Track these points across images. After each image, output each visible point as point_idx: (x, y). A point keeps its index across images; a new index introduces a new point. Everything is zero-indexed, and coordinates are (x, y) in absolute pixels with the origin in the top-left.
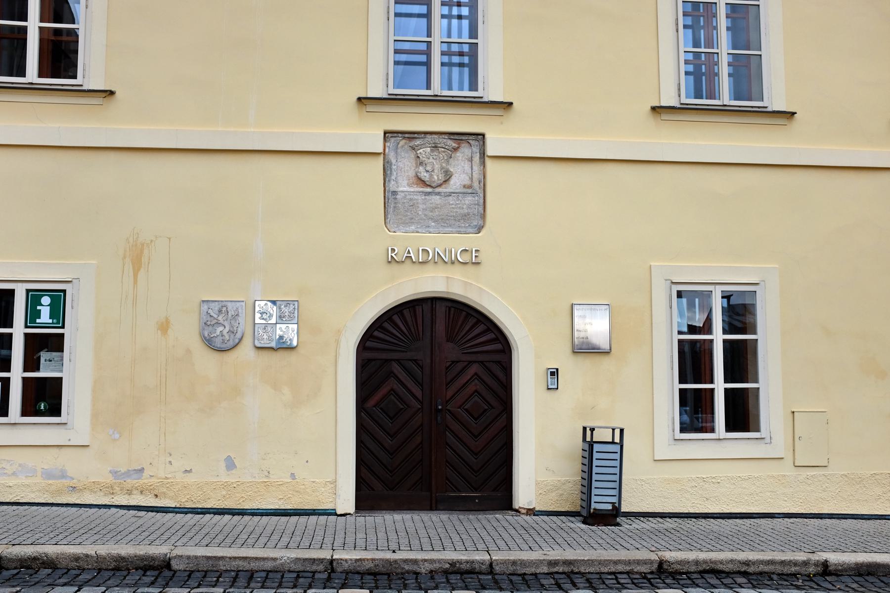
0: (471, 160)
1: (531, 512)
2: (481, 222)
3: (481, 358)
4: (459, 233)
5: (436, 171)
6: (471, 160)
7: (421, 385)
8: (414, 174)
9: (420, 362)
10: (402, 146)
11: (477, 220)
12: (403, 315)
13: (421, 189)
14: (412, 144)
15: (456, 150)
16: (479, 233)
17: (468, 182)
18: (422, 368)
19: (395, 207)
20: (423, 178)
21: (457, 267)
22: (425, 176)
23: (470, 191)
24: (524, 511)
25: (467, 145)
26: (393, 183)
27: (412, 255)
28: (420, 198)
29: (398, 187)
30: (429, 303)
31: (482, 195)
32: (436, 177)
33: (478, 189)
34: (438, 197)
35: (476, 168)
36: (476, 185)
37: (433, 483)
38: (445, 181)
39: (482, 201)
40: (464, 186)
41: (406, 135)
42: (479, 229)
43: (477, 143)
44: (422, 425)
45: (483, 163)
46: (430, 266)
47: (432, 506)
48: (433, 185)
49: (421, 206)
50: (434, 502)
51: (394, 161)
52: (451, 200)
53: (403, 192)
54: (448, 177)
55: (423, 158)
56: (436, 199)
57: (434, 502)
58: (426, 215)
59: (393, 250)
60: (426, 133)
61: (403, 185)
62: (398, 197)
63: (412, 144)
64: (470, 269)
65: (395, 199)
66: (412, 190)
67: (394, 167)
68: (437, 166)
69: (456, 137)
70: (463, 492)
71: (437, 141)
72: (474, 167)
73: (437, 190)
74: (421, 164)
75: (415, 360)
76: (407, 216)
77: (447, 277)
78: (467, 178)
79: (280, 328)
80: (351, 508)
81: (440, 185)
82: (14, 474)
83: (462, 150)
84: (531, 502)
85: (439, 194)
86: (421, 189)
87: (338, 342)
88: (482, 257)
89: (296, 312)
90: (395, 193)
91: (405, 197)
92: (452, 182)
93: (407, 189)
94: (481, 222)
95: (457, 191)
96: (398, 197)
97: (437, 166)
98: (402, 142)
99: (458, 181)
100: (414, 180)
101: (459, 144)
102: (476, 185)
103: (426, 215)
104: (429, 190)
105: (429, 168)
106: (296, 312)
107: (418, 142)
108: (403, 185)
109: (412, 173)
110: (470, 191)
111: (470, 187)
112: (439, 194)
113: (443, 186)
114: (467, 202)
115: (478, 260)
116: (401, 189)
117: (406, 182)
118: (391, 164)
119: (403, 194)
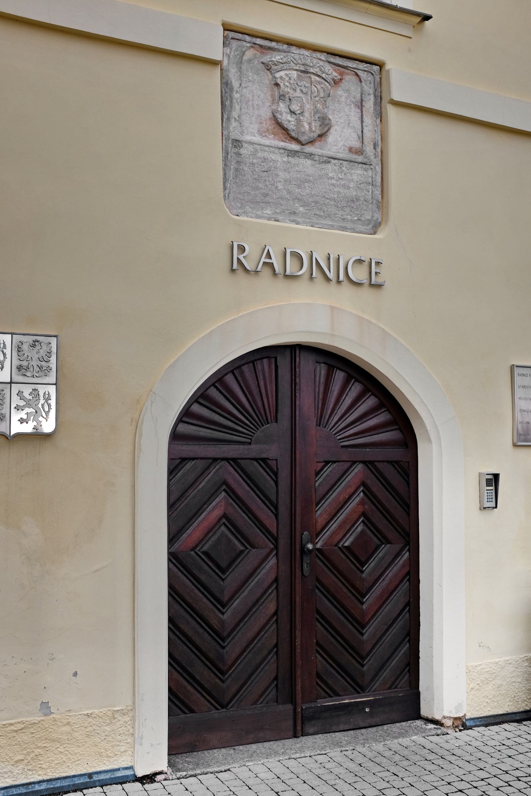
0: (361, 105)
1: (463, 724)
2: (377, 216)
3: (370, 454)
4: (344, 229)
5: (307, 114)
6: (361, 105)
7: (275, 507)
8: (269, 115)
9: (273, 464)
10: (250, 61)
11: (373, 212)
12: (242, 374)
13: (282, 144)
14: (266, 59)
15: (336, 83)
16: (375, 233)
17: (356, 144)
18: (276, 474)
19: (237, 170)
20: (286, 124)
21: (346, 289)
22: (287, 119)
23: (360, 159)
24: (449, 723)
25: (354, 78)
26: (234, 124)
27: (274, 260)
28: (280, 159)
29: (242, 133)
30: (288, 353)
31: (379, 168)
32: (307, 127)
33: (372, 156)
34: (309, 162)
35: (368, 120)
36: (369, 149)
37: (299, 687)
38: (320, 136)
39: (379, 179)
40: (350, 150)
41: (259, 41)
42: (375, 228)
43: (370, 78)
44: (276, 580)
45: (380, 115)
46: (303, 285)
47: (299, 726)
48: (303, 139)
49: (282, 175)
50: (299, 722)
51: (235, 84)
52: (330, 169)
53: (251, 143)
54: (326, 127)
55: (285, 87)
56: (306, 166)
57: (299, 722)
58: (289, 192)
59: (242, 249)
60: (290, 43)
61: (252, 131)
62: (243, 151)
63: (266, 59)
64: (366, 293)
65: (239, 154)
66: (267, 142)
67: (236, 96)
68: (308, 107)
69: (338, 61)
70: (346, 693)
71: (308, 62)
72: (366, 119)
73: (309, 149)
74: (282, 97)
75: (264, 460)
76: (257, 188)
77: (332, 308)
78: (355, 136)
79: (20, 393)
80: (162, 765)
81: (311, 142)
82: (292, 112)
83: (344, 85)
84: (460, 705)
85: (310, 156)
86: (282, 144)
87: (137, 425)
88: (385, 276)
89: (53, 359)
90: (237, 143)
91: (254, 154)
92: (331, 138)
93: (256, 139)
94: (377, 216)
95: (340, 156)
96: (243, 151)
97: (308, 107)
98: (249, 54)
99: (341, 138)
100: (269, 125)
101: (341, 74)
102: (369, 149)
103: (289, 192)
104: (295, 147)
105: (295, 107)
106: (53, 359)
107: (277, 57)
108: (252, 131)
109: (266, 113)
110: (360, 159)
111: (360, 152)
112: (310, 156)
113: (318, 144)
114: (355, 178)
115: (380, 280)
116: (248, 138)
117: (254, 127)
118: (232, 89)
119: (251, 148)
